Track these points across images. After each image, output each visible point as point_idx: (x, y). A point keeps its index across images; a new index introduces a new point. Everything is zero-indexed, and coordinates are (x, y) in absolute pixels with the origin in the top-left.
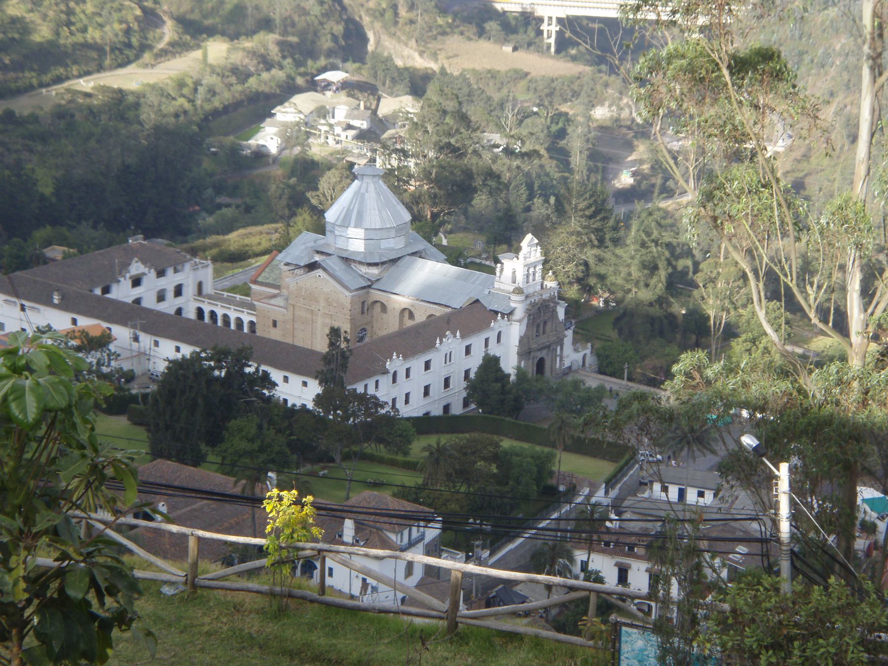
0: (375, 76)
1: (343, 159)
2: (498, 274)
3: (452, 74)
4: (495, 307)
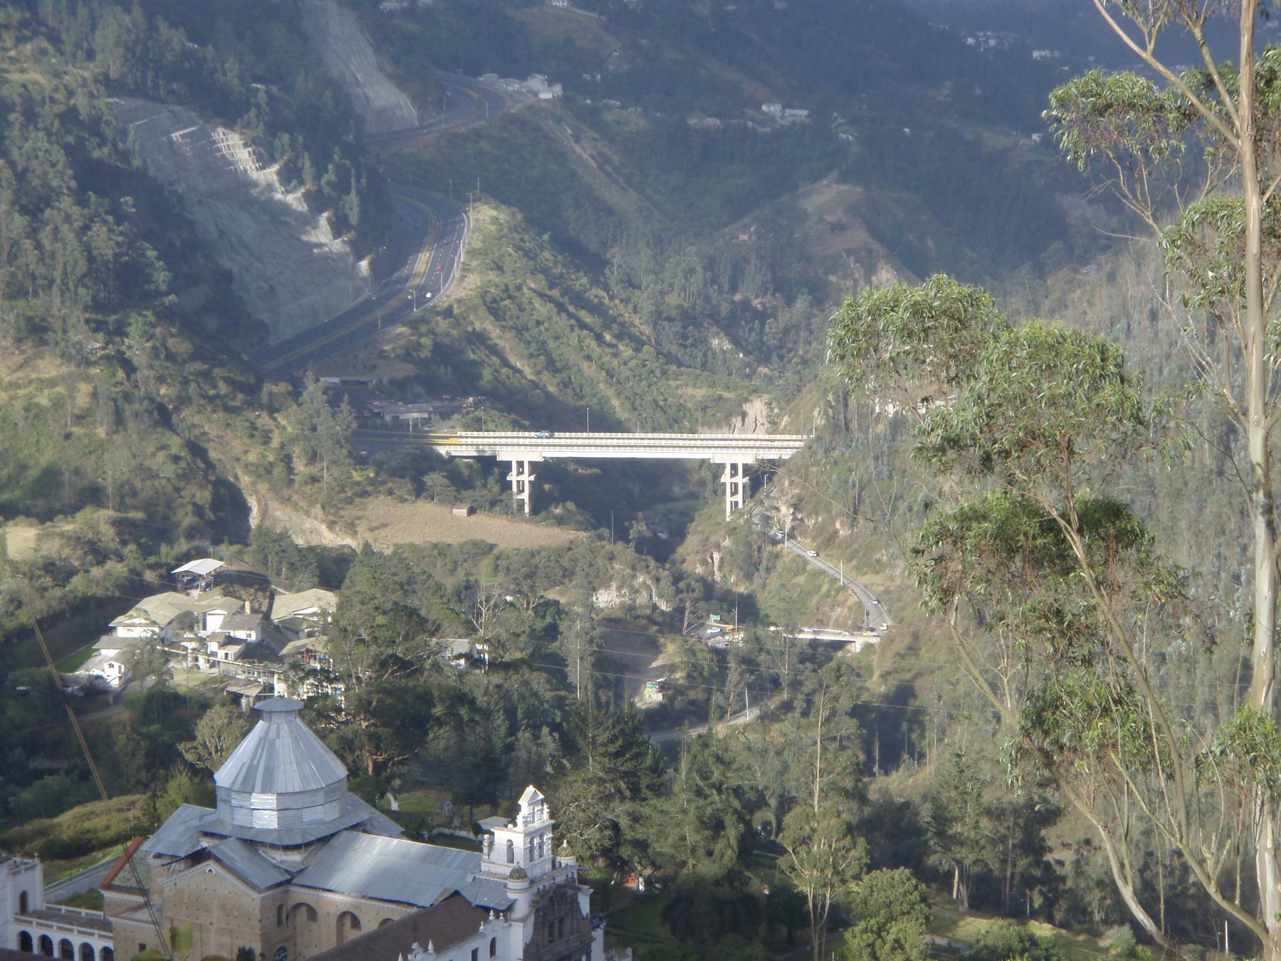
0: (265, 562)
1: (223, 689)
2: (486, 850)
3: (381, 554)
4: (484, 901)
